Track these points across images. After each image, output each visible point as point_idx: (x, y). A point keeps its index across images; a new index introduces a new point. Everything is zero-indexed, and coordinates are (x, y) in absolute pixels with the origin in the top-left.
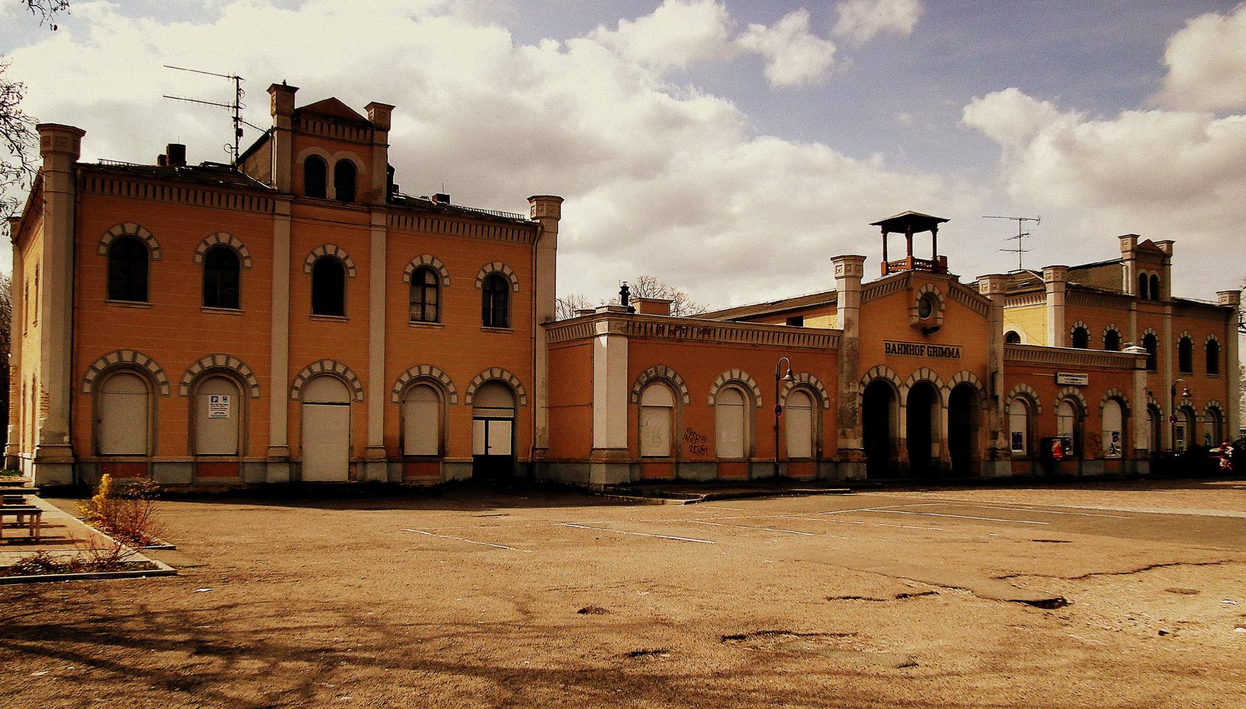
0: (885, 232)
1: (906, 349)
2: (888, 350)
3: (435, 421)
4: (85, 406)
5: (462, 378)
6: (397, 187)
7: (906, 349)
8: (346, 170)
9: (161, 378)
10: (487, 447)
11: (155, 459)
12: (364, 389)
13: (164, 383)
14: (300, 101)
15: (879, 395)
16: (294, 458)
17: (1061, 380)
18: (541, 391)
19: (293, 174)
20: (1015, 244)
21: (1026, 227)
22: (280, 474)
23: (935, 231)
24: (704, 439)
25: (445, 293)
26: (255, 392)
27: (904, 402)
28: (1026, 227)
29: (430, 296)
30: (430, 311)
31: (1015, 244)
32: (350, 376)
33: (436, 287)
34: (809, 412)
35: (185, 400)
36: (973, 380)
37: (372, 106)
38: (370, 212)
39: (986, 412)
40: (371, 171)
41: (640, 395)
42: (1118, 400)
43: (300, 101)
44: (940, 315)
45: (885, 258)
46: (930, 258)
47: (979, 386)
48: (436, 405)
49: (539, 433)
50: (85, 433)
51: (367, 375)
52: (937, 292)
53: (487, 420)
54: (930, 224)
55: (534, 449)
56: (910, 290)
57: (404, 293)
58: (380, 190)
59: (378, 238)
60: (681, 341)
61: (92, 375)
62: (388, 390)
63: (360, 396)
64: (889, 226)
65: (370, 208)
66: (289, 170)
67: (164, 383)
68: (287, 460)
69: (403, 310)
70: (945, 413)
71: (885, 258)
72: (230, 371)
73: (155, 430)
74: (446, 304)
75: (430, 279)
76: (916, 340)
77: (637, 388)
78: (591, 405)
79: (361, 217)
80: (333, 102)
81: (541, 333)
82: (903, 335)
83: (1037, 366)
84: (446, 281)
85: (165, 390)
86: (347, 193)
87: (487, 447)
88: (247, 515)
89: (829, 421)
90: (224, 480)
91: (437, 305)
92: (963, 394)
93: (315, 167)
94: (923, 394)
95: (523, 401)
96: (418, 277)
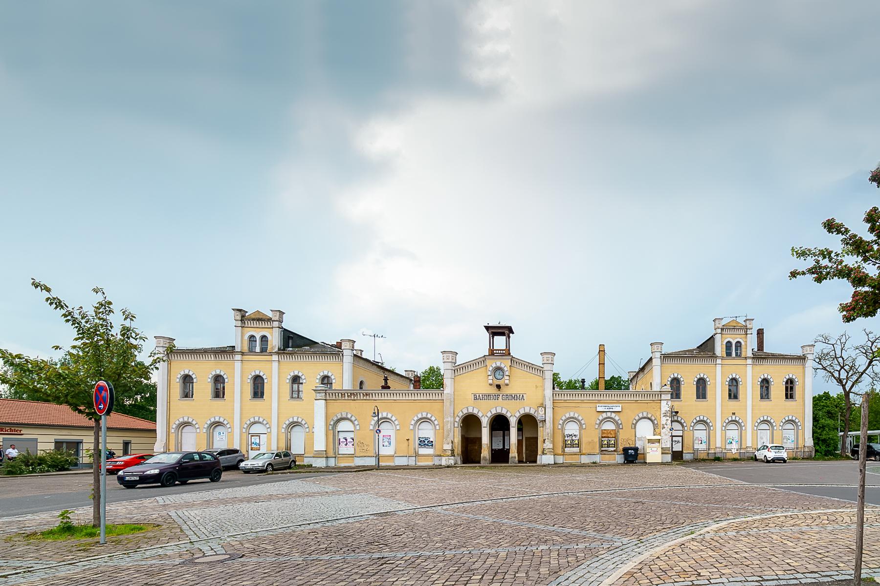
1: (488, 396)
2: (476, 398)
15: (470, 422)
17: (599, 409)
59: (275, 365)
61: (174, 426)
65: (271, 354)
76: (493, 391)
93: (252, 337)
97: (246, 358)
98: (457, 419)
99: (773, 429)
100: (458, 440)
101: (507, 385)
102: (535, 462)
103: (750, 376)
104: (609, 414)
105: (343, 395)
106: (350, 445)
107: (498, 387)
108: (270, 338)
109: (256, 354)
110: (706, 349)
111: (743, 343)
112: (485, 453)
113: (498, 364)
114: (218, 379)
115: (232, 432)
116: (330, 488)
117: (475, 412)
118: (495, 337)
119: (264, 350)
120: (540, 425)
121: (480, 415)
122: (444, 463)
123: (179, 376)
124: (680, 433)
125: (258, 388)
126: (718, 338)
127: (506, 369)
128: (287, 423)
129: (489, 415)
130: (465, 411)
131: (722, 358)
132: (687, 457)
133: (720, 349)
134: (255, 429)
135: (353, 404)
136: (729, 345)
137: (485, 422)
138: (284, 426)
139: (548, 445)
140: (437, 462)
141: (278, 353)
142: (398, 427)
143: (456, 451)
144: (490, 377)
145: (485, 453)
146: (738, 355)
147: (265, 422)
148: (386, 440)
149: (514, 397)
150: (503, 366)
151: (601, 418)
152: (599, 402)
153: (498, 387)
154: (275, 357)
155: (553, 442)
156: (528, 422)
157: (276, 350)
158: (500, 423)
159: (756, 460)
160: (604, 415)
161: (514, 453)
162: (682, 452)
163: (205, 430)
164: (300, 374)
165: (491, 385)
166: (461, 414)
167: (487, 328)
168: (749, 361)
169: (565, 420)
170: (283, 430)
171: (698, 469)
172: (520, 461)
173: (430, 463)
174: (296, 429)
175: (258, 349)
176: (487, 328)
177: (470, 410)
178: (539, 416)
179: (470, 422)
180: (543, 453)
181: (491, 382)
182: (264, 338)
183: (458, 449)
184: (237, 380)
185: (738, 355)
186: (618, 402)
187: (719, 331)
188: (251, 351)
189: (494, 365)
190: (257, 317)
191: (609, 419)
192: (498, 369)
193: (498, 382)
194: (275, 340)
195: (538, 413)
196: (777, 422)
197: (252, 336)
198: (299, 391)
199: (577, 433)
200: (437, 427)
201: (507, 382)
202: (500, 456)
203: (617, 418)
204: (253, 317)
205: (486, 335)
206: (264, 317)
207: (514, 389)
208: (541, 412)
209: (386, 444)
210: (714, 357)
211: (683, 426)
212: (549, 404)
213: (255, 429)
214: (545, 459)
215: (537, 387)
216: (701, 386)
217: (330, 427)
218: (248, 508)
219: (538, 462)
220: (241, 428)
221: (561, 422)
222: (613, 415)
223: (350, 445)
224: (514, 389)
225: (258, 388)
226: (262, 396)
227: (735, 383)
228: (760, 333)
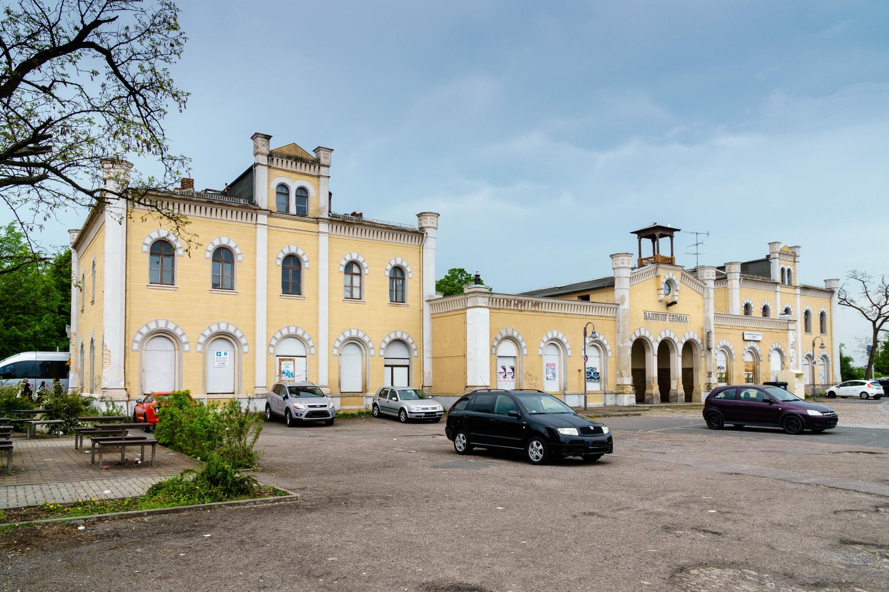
0: (640, 238)
1: (656, 316)
2: (646, 318)
3: (360, 369)
4: (133, 358)
5: (377, 340)
7: (656, 316)
9: (184, 339)
12: (316, 346)
13: (187, 343)
15: (640, 347)
18: (427, 347)
20: (693, 250)
21: (701, 238)
23: (672, 237)
24: (536, 378)
25: (365, 279)
26: (246, 349)
27: (656, 353)
28: (701, 238)
29: (356, 280)
30: (356, 294)
31: (693, 250)
33: (360, 275)
34: (598, 359)
35: (201, 355)
36: (696, 338)
38: (318, 223)
39: (703, 359)
40: (318, 194)
41: (496, 348)
42: (779, 351)
44: (676, 293)
45: (640, 256)
47: (699, 341)
48: (360, 357)
49: (426, 375)
50: (134, 379)
51: (317, 336)
52: (674, 278)
53: (392, 366)
54: (668, 232)
56: (658, 277)
57: (342, 279)
58: (325, 208)
60: (521, 311)
61: (139, 337)
62: (331, 346)
63: (313, 351)
64: (642, 234)
65: (317, 220)
66: (266, 193)
67: (187, 343)
69: (341, 292)
70: (655, 359)
71: (640, 256)
73: (180, 377)
74: (366, 287)
75: (355, 270)
76: (661, 309)
77: (495, 344)
78: (465, 356)
79: (312, 226)
81: (426, 306)
84: (367, 271)
85: (187, 347)
88: (756, 443)
90: (353, 407)
91: (360, 287)
92: (689, 346)
93: (283, 190)
94: (665, 347)
95: (416, 353)
96: (351, 267)
97: (275, 221)
103: (323, 254)
105: (509, 302)
106: (509, 376)
109: (292, 217)
110: (240, 193)
114: (398, 273)
118: (643, 239)
125: (292, 273)
126: (261, 174)
131: (270, 213)
133: (264, 192)
135: (519, 316)
136: (283, 190)
146: (302, 213)
148: (550, 371)
159: (868, 397)
168: (798, 291)
175: (293, 209)
184: (324, 265)
185: (302, 213)
186: (758, 329)
187: (263, 160)
190: (293, 153)
193: (669, 299)
196: (193, 334)
197: (283, 186)
199: (724, 365)
204: (286, 151)
206: (304, 156)
209: (550, 376)
210: (251, 206)
215: (698, 307)
223: (509, 376)
225: (292, 273)
227: (399, 275)
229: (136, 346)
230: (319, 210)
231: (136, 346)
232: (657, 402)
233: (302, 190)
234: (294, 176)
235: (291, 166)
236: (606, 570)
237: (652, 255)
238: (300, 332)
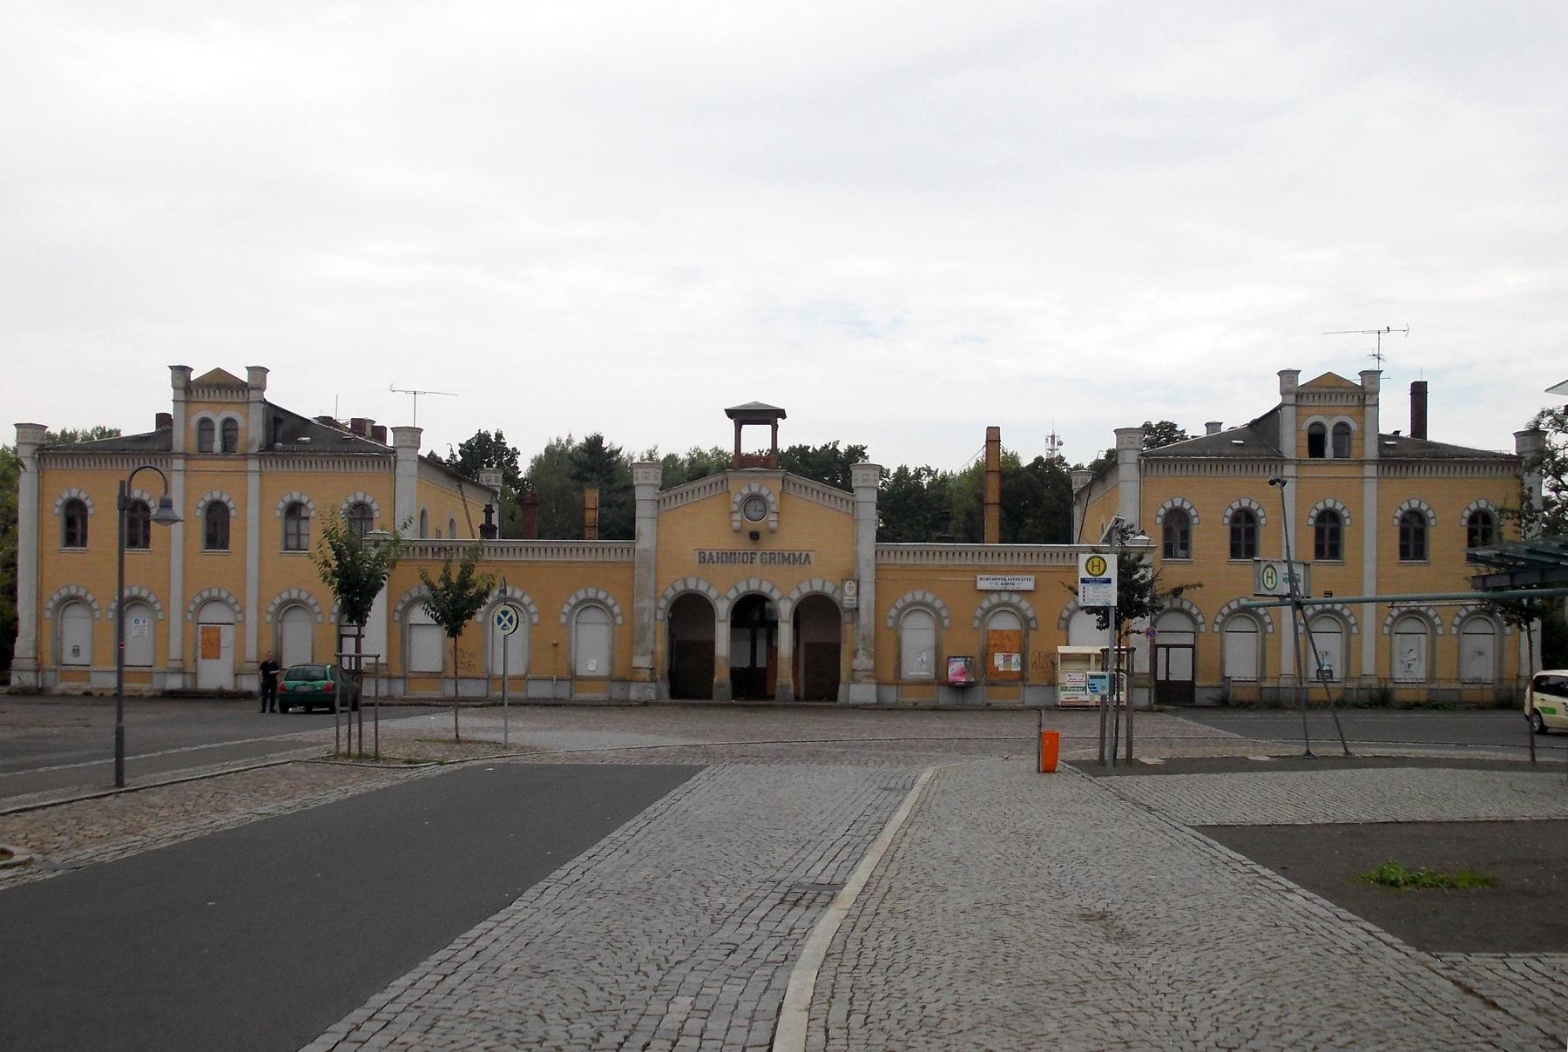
1: (729, 557)
2: (702, 560)
6: (63, 432)
8: (1342, 430)
10: (1168, 673)
11: (93, 668)
14: (194, 376)
15: (689, 610)
16: (190, 669)
17: (982, 585)
19: (186, 435)
22: (175, 683)
32: (232, 600)
37: (1362, 374)
43: (1302, 380)
46: (730, 448)
53: (1168, 647)
55: (1519, 677)
59: (253, 481)
61: (51, 605)
65: (246, 457)
68: (182, 671)
72: (73, 597)
76: (744, 545)
80: (219, 371)
82: (722, 541)
83: (944, 570)
86: (229, 445)
87: (1168, 673)
89: (625, 640)
93: (205, 425)
97: (193, 464)
98: (663, 604)
99: (1434, 632)
100: (662, 647)
101: (772, 532)
102: (835, 698)
104: (1005, 597)
107: (754, 536)
108: (241, 422)
109: (215, 457)
111: (1354, 426)
112: (722, 675)
113: (755, 488)
115: (167, 620)
116: (521, 725)
117: (702, 587)
119: (229, 445)
120: (846, 618)
121: (712, 594)
122: (634, 694)
123: (60, 502)
124: (1188, 639)
125: (217, 527)
127: (771, 498)
128: (278, 601)
129: (733, 595)
130: (680, 587)
131: (187, 456)
132: (1201, 696)
133: (1291, 441)
134: (212, 614)
137: (723, 609)
138: (272, 609)
139: (864, 662)
140: (617, 691)
141: (260, 456)
142: (535, 619)
143: (659, 669)
144: (737, 517)
145: (722, 675)
147: (232, 600)
149: (791, 559)
150: (764, 492)
151: (986, 604)
152: (984, 570)
153: (754, 536)
154: (253, 465)
155: (876, 657)
156: (819, 612)
157: (255, 449)
158: (752, 614)
160: (994, 599)
161: (785, 675)
162: (1190, 686)
163: (110, 615)
164: (304, 499)
165: (737, 531)
166: (670, 593)
167: (731, 413)
168: (1371, 470)
169: (903, 609)
170: (269, 618)
171: (1218, 726)
172: (797, 698)
173: (600, 696)
174: (297, 615)
175: (217, 446)
176: (731, 413)
177: (692, 585)
178: (847, 597)
179: (689, 610)
180: (854, 680)
181: (737, 525)
182: (229, 424)
183: (663, 665)
186: (1026, 570)
187: (1291, 399)
188: (204, 450)
189: (745, 491)
191: (1004, 608)
192: (753, 498)
193: (753, 526)
194: (253, 430)
195: (843, 593)
198: (299, 535)
200: (619, 620)
201: (773, 525)
202: (752, 687)
203: (1024, 605)
205: (730, 424)
207: (790, 539)
208: (849, 589)
210: (1279, 459)
211: (1195, 622)
212: (867, 575)
213: (212, 614)
214: (861, 692)
216: (1244, 535)
217: (397, 617)
218: (20, 802)
219: (841, 700)
220: (185, 611)
221: (893, 613)
222: (1015, 599)
224: (790, 539)
226: (225, 545)
228: (1419, 392)
229: (48, 614)
230: (248, 444)
231: (48, 614)
232: (1471, 551)
233: (229, 424)
234: (219, 407)
235: (217, 396)
236: (646, 950)
237: (1095, 720)
238: (215, 593)
